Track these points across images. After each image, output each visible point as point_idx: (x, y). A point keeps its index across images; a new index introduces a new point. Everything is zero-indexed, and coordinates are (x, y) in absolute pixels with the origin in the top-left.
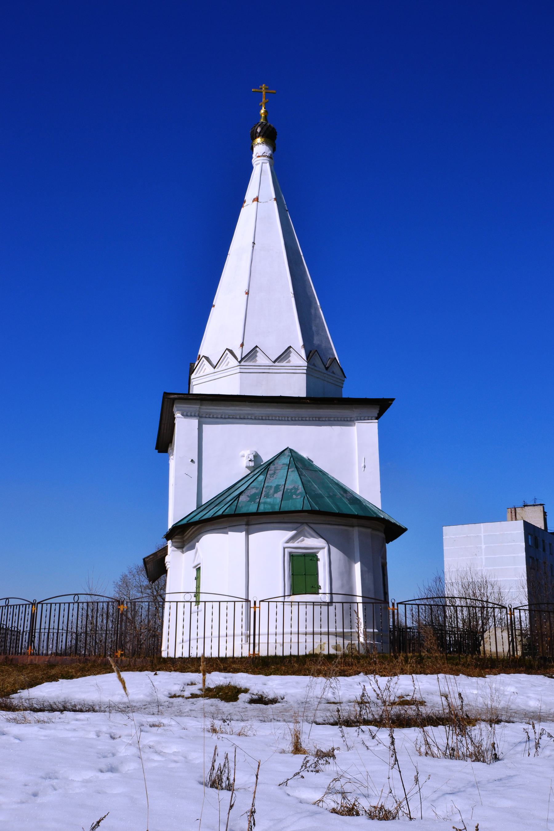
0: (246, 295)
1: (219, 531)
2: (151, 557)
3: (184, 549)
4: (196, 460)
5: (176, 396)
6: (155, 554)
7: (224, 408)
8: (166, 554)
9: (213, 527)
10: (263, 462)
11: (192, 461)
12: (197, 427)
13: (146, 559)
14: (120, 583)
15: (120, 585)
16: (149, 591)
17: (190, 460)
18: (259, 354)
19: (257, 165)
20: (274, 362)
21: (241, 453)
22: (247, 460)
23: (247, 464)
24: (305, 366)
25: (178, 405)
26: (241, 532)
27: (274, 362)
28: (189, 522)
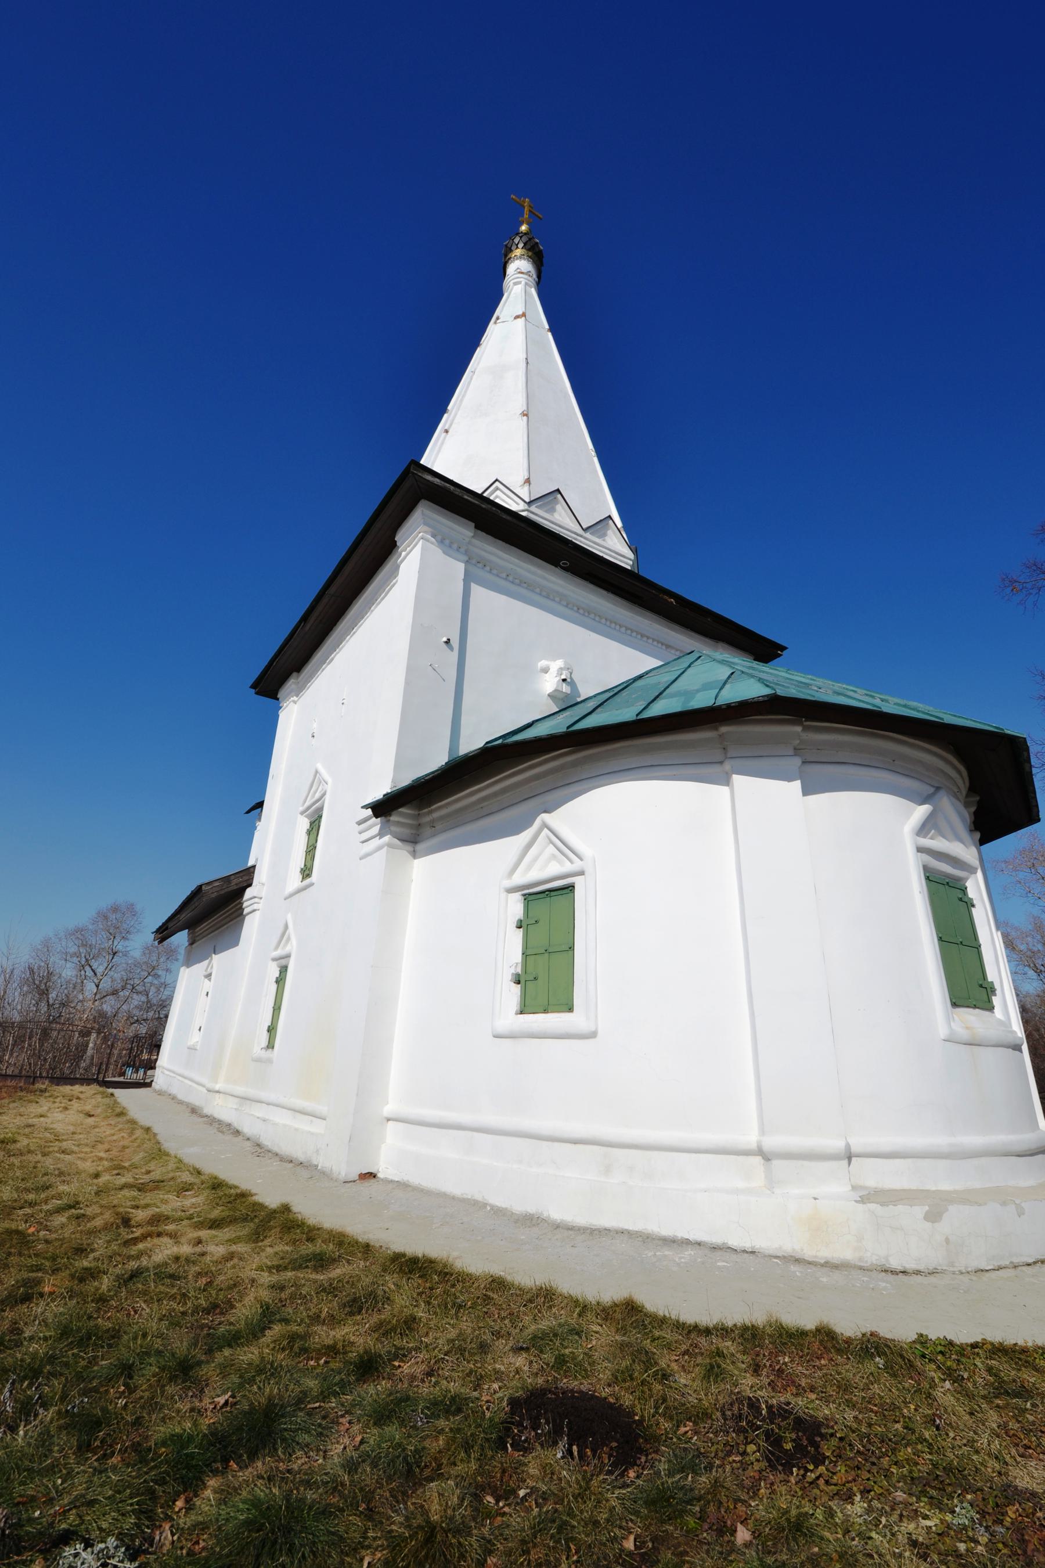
0: (525, 418)
1: (668, 771)
2: (217, 884)
3: (420, 847)
4: (455, 643)
5: (438, 480)
6: (227, 879)
7: (516, 561)
8: (249, 882)
9: (648, 759)
10: (579, 697)
11: (448, 642)
12: (462, 577)
13: (203, 887)
14: (39, 947)
15: (38, 949)
16: (75, 960)
17: (445, 639)
18: (560, 507)
19: (515, 284)
20: (585, 530)
21: (543, 663)
22: (558, 679)
23: (557, 686)
24: (630, 560)
25: (427, 512)
26: (790, 779)
27: (585, 530)
28: (571, 729)
